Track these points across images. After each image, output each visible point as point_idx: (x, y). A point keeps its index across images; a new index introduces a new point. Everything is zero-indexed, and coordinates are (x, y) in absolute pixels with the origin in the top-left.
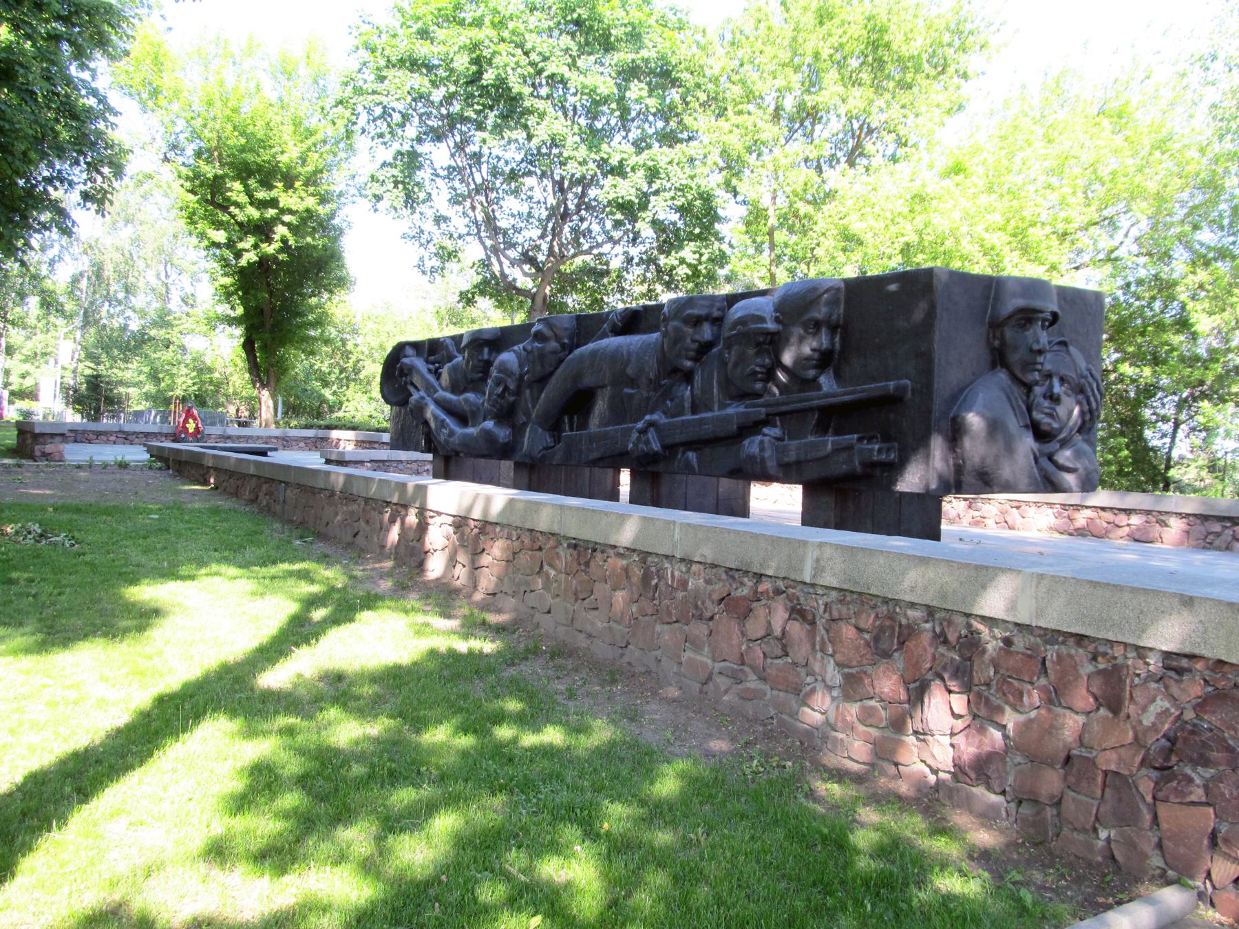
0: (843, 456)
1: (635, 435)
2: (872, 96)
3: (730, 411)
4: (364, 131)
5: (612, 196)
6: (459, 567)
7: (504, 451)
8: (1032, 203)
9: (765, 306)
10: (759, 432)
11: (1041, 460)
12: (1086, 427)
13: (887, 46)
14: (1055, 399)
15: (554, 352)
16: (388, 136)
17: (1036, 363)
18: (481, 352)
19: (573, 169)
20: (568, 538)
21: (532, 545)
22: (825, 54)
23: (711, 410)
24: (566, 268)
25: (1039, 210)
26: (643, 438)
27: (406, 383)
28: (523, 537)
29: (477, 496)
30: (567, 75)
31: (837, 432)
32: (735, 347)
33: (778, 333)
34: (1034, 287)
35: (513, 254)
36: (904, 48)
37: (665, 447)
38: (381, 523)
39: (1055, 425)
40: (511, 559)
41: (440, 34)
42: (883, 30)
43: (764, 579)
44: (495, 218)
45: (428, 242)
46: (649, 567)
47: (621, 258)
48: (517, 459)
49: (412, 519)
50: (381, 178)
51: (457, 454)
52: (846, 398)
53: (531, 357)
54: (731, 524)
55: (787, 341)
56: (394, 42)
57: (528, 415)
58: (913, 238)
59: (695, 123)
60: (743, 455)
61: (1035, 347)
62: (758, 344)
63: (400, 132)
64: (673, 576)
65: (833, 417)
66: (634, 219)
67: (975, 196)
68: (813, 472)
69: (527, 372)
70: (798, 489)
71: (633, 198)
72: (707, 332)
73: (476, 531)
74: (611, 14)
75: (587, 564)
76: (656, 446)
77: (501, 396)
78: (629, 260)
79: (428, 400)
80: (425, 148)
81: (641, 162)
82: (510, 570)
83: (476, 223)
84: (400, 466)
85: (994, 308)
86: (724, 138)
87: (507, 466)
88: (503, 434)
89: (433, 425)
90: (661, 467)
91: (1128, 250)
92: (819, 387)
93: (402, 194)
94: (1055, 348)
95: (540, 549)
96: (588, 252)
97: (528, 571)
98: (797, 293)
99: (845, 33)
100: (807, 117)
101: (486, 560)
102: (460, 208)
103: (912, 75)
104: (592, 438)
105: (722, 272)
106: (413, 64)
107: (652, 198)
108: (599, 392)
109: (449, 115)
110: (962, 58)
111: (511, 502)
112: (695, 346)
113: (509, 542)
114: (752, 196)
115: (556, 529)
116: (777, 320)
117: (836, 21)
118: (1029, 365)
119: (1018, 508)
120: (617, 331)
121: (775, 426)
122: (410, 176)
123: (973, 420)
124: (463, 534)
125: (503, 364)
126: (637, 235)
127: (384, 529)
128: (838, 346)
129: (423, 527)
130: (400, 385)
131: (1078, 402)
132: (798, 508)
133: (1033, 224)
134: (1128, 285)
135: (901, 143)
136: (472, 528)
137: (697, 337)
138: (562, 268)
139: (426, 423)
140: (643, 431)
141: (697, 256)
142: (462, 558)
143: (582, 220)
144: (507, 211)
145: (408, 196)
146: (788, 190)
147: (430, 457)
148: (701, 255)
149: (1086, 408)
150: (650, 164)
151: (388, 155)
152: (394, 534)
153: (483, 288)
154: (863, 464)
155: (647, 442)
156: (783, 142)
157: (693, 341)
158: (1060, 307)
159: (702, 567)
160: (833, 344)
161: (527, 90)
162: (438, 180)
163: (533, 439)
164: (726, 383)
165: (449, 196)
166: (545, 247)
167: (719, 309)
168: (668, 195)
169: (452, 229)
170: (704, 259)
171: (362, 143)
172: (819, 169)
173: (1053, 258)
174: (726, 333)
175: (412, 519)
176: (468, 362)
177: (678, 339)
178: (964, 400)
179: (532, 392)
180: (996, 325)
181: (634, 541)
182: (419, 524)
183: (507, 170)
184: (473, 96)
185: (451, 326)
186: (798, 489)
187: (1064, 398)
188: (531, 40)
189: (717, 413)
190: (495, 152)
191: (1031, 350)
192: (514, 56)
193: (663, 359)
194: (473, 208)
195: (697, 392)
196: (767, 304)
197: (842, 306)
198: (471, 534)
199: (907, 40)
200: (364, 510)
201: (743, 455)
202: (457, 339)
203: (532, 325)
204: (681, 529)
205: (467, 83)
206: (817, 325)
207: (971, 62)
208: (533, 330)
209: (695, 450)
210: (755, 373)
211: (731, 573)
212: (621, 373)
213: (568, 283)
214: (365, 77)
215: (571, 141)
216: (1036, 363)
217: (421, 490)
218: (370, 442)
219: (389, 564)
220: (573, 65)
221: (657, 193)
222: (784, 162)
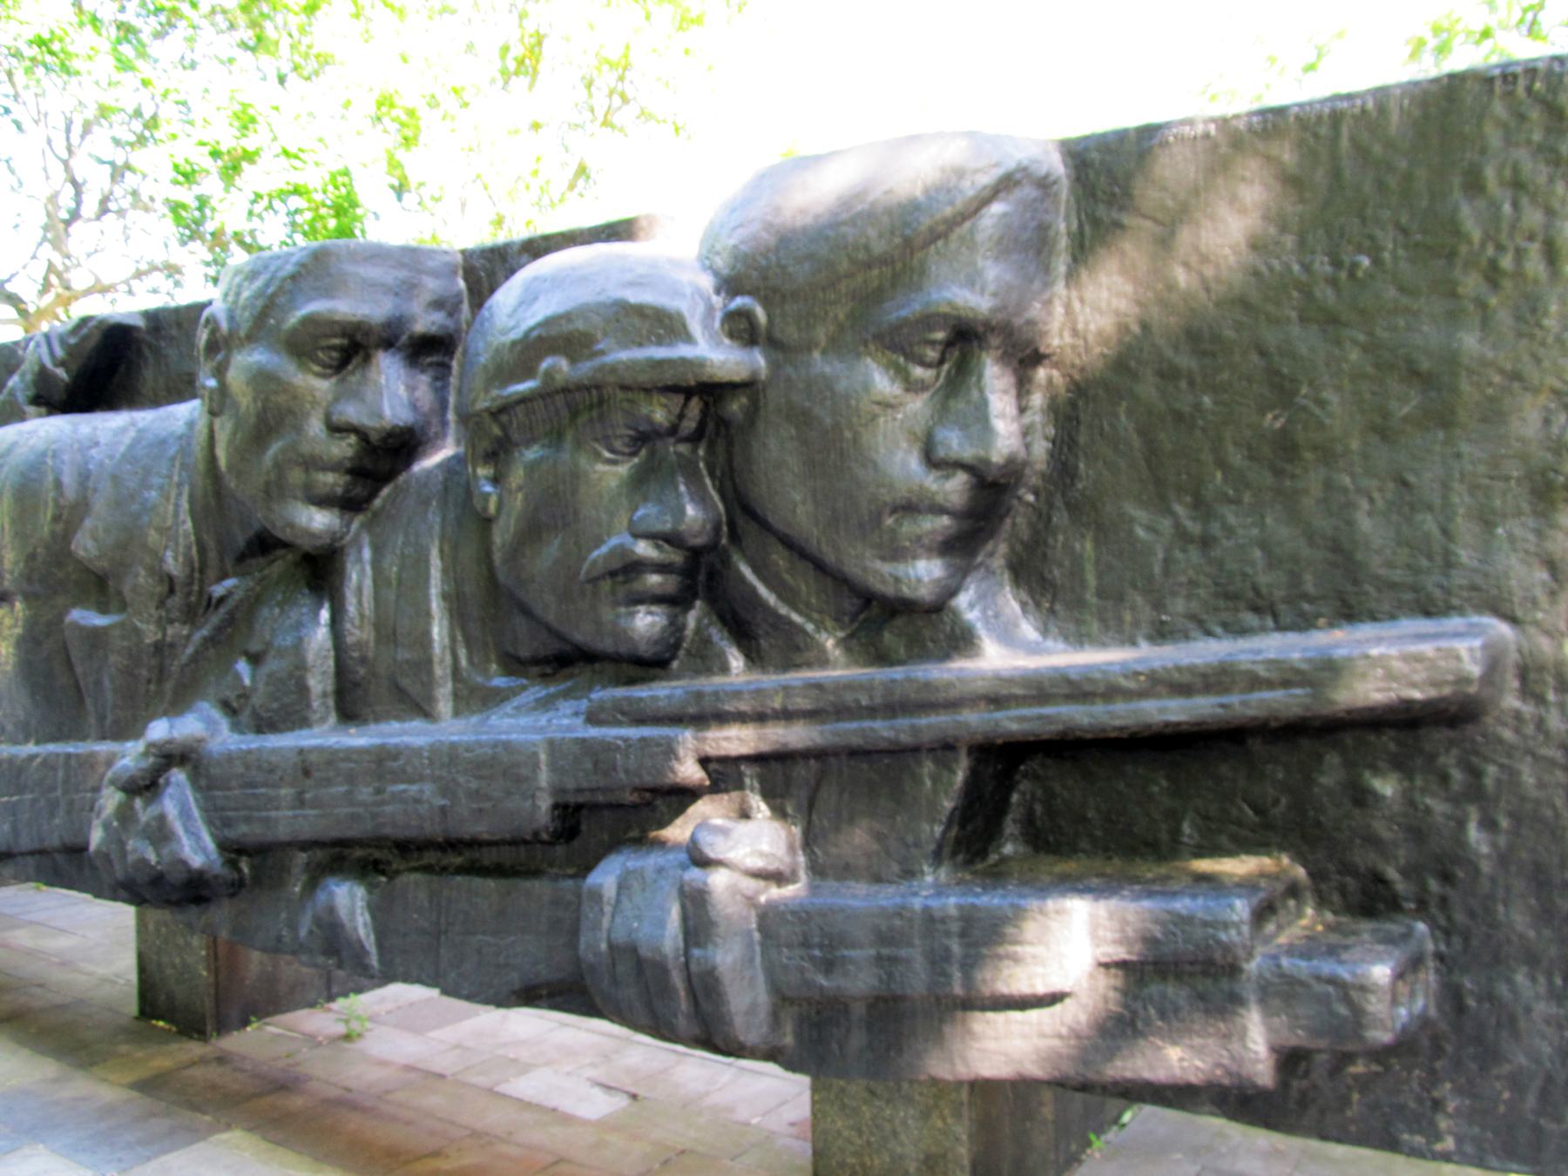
1: (111, 800)
23: (422, 708)
26: (144, 812)
37: (232, 850)
62: (644, 437)
72: (392, 393)
112: (343, 449)
116: (741, 329)
128: (1041, 449)
132: (806, 1098)
137: (351, 412)
140: (146, 786)
155: (160, 833)
157: (336, 429)
167: (438, 304)
177: (271, 419)
193: (214, 497)
195: (358, 633)
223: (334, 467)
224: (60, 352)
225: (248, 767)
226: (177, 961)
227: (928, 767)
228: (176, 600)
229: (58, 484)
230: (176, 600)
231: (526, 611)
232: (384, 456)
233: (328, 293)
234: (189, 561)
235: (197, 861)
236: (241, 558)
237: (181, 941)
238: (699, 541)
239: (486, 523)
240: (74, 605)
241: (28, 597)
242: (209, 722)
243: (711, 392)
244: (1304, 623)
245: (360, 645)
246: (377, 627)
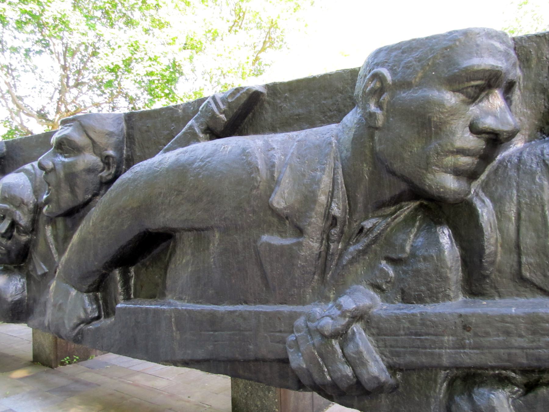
15: (90, 170)
53: (52, 178)
69: (47, 202)
120: (213, 132)
225: (412, 322)
226: (259, 403)
234: (344, 211)
237: (261, 394)
240: (264, 233)
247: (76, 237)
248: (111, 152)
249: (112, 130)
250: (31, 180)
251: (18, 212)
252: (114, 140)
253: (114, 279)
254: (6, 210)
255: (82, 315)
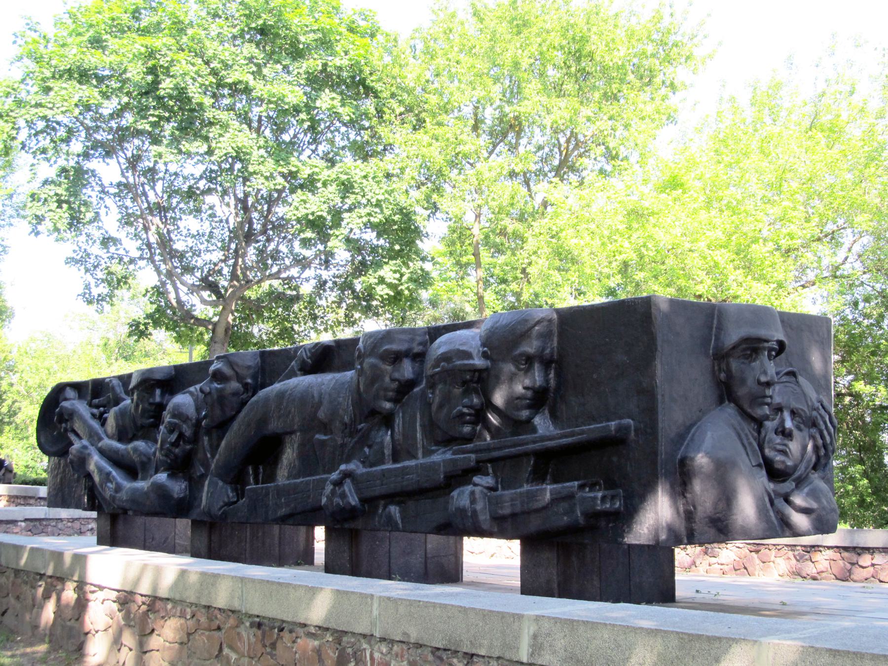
0: (563, 506)
1: (329, 488)
2: (577, 106)
3: (437, 458)
4: (24, 146)
5: (301, 212)
6: (125, 650)
7: (180, 508)
8: (751, 219)
9: (470, 340)
10: (469, 482)
11: (776, 502)
12: (821, 463)
13: (591, 55)
14: (787, 435)
15: (235, 394)
16: (51, 152)
17: (765, 397)
18: (152, 394)
19: (260, 185)
20: (250, 616)
21: (209, 624)
22: (525, 63)
23: (415, 457)
24: (252, 294)
25: (760, 226)
26: (338, 491)
27: (66, 430)
28: (198, 615)
29: (144, 567)
30: (252, 83)
31: (555, 481)
32: (440, 386)
33: (487, 370)
34: (760, 314)
35: (189, 279)
36: (607, 58)
37: (363, 501)
38: (34, 599)
39: (790, 463)
40: (186, 641)
41: (113, 43)
42: (584, 40)
43: (475, 659)
44: (171, 240)
45: (95, 267)
46: (344, 649)
47: (313, 282)
48: (194, 516)
49: (69, 594)
50: (43, 196)
51: (125, 511)
52: (565, 441)
53: (209, 399)
54: (438, 595)
55: (497, 380)
56: (62, 51)
57: (207, 466)
58: (631, 256)
59: (391, 135)
60: (452, 508)
61: (763, 379)
62: (464, 383)
63: (64, 146)
64: (372, 658)
65: (550, 462)
66: (324, 238)
67: (695, 211)
68: (535, 524)
69: (205, 417)
70: (516, 544)
71: (325, 214)
72: (407, 370)
73: (144, 608)
74: (300, 22)
75: (273, 646)
76: (353, 500)
77: (175, 444)
78: (322, 284)
79: (92, 450)
80: (94, 164)
81: (334, 176)
82: (185, 654)
83: (149, 246)
84: (60, 525)
85: (717, 339)
86: (424, 151)
87: (183, 526)
88: (178, 488)
89: (97, 478)
90: (359, 524)
91: (853, 268)
92: (534, 430)
93: (67, 215)
94: (784, 379)
95: (219, 628)
96: (276, 276)
97: (206, 655)
98: (506, 325)
99: (544, 41)
100: (508, 130)
101: (155, 642)
102: (132, 230)
103: (617, 86)
104: (281, 492)
105: (425, 295)
106: (83, 75)
107: (345, 215)
108: (287, 439)
109: (120, 128)
110: (669, 70)
111: (183, 573)
112: (395, 385)
113: (182, 621)
114: (454, 211)
115: (236, 605)
116: (485, 355)
117: (534, 30)
118: (758, 399)
119: (757, 552)
121: (487, 474)
122: (76, 195)
123: (701, 460)
124: (128, 613)
125: (177, 407)
126: (330, 254)
127: (37, 606)
128: (552, 383)
129: (82, 604)
130: (59, 433)
131: (812, 437)
132: (517, 561)
133: (755, 241)
134: (856, 304)
135: (611, 156)
136: (139, 605)
137: (396, 375)
138: (247, 293)
139: (89, 476)
140: (338, 483)
141: (398, 276)
142: (128, 639)
143: (269, 240)
144: (185, 232)
145: (72, 218)
146: (494, 204)
147: (94, 514)
148: (402, 275)
149: (820, 442)
150: (344, 177)
151: (48, 171)
152: (49, 612)
153: (157, 319)
154: (586, 515)
155: (343, 496)
156: (486, 155)
157: (393, 380)
158: (787, 335)
159: (405, 647)
160: (547, 381)
161: (208, 101)
162: (106, 198)
163: (212, 494)
164: (430, 427)
165: (120, 216)
166: (226, 271)
168: (363, 211)
169: (121, 252)
170: (405, 278)
171: (23, 159)
172: (527, 183)
173: (779, 276)
174: (429, 370)
175: (69, 594)
176: (137, 406)
177: (375, 377)
178: (692, 439)
179: (210, 440)
180: (721, 356)
181: (327, 619)
182: (78, 600)
183: (185, 188)
184: (147, 108)
185: (122, 362)
186: (516, 544)
187: (796, 432)
188: (212, 48)
189: (421, 461)
190: (173, 168)
191: (759, 383)
192: (193, 65)
193: (359, 399)
194: (146, 229)
196: (473, 338)
197: (556, 339)
198: (140, 614)
199: (610, 50)
200: (13, 583)
201: (452, 508)
202: (125, 379)
203: (210, 363)
204: (383, 600)
205: (142, 94)
206: (529, 360)
207: (680, 73)
208: (212, 368)
209: (398, 504)
210: (462, 415)
211: (439, 653)
212: (311, 416)
213: (254, 310)
214: (29, 88)
215: (256, 154)
216: (765, 397)
217: (80, 560)
218: (25, 498)
219: (42, 648)
220: (258, 73)
221: (350, 210)
222: (487, 175)
223: (393, 390)
224: (309, 354)
227: (525, 460)
228: (347, 430)
229: (313, 397)
230: (347, 430)
231: (439, 427)
232: (405, 387)
233: (391, 343)
234: (351, 419)
235: (353, 503)
236: (366, 417)
238: (478, 407)
239: (430, 405)
241: (301, 431)
242: (357, 466)
243: (480, 371)
244: (601, 422)
245: (398, 440)
246: (403, 435)
247: (223, 443)
248: (249, 381)
249: (250, 364)
250: (195, 401)
251: (184, 426)
252: (251, 371)
253: (248, 473)
254: (176, 424)
255: (226, 500)
